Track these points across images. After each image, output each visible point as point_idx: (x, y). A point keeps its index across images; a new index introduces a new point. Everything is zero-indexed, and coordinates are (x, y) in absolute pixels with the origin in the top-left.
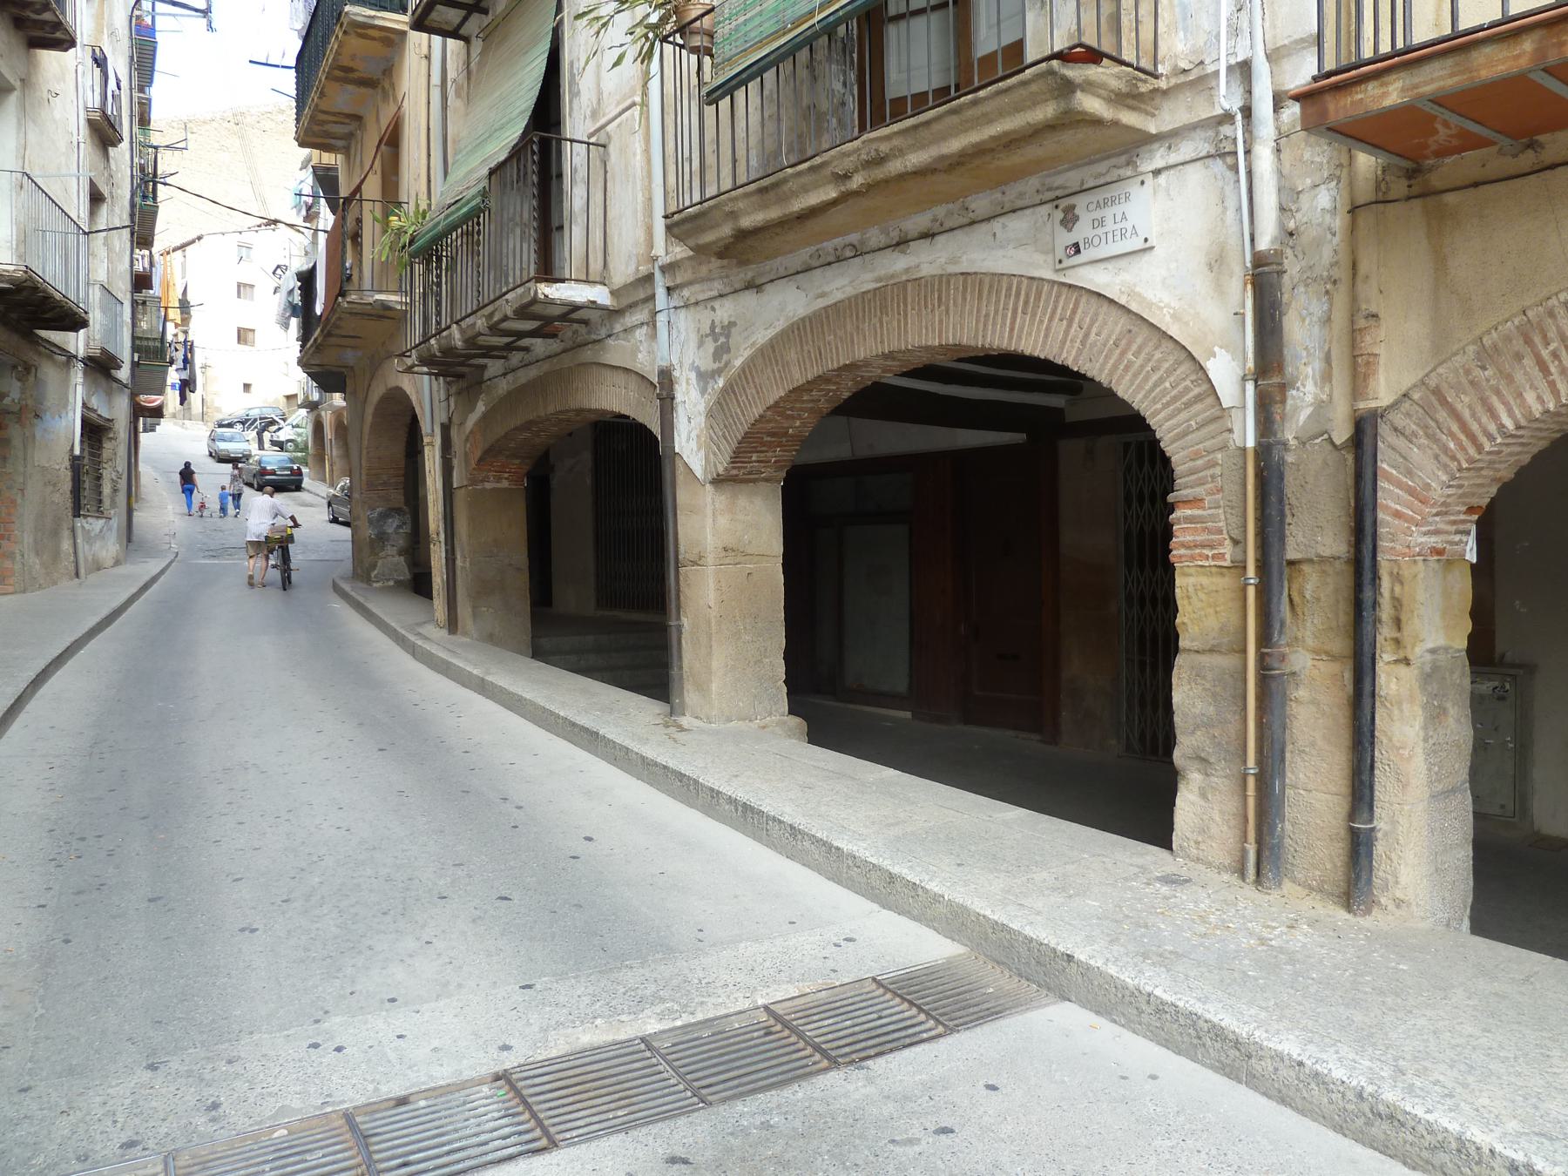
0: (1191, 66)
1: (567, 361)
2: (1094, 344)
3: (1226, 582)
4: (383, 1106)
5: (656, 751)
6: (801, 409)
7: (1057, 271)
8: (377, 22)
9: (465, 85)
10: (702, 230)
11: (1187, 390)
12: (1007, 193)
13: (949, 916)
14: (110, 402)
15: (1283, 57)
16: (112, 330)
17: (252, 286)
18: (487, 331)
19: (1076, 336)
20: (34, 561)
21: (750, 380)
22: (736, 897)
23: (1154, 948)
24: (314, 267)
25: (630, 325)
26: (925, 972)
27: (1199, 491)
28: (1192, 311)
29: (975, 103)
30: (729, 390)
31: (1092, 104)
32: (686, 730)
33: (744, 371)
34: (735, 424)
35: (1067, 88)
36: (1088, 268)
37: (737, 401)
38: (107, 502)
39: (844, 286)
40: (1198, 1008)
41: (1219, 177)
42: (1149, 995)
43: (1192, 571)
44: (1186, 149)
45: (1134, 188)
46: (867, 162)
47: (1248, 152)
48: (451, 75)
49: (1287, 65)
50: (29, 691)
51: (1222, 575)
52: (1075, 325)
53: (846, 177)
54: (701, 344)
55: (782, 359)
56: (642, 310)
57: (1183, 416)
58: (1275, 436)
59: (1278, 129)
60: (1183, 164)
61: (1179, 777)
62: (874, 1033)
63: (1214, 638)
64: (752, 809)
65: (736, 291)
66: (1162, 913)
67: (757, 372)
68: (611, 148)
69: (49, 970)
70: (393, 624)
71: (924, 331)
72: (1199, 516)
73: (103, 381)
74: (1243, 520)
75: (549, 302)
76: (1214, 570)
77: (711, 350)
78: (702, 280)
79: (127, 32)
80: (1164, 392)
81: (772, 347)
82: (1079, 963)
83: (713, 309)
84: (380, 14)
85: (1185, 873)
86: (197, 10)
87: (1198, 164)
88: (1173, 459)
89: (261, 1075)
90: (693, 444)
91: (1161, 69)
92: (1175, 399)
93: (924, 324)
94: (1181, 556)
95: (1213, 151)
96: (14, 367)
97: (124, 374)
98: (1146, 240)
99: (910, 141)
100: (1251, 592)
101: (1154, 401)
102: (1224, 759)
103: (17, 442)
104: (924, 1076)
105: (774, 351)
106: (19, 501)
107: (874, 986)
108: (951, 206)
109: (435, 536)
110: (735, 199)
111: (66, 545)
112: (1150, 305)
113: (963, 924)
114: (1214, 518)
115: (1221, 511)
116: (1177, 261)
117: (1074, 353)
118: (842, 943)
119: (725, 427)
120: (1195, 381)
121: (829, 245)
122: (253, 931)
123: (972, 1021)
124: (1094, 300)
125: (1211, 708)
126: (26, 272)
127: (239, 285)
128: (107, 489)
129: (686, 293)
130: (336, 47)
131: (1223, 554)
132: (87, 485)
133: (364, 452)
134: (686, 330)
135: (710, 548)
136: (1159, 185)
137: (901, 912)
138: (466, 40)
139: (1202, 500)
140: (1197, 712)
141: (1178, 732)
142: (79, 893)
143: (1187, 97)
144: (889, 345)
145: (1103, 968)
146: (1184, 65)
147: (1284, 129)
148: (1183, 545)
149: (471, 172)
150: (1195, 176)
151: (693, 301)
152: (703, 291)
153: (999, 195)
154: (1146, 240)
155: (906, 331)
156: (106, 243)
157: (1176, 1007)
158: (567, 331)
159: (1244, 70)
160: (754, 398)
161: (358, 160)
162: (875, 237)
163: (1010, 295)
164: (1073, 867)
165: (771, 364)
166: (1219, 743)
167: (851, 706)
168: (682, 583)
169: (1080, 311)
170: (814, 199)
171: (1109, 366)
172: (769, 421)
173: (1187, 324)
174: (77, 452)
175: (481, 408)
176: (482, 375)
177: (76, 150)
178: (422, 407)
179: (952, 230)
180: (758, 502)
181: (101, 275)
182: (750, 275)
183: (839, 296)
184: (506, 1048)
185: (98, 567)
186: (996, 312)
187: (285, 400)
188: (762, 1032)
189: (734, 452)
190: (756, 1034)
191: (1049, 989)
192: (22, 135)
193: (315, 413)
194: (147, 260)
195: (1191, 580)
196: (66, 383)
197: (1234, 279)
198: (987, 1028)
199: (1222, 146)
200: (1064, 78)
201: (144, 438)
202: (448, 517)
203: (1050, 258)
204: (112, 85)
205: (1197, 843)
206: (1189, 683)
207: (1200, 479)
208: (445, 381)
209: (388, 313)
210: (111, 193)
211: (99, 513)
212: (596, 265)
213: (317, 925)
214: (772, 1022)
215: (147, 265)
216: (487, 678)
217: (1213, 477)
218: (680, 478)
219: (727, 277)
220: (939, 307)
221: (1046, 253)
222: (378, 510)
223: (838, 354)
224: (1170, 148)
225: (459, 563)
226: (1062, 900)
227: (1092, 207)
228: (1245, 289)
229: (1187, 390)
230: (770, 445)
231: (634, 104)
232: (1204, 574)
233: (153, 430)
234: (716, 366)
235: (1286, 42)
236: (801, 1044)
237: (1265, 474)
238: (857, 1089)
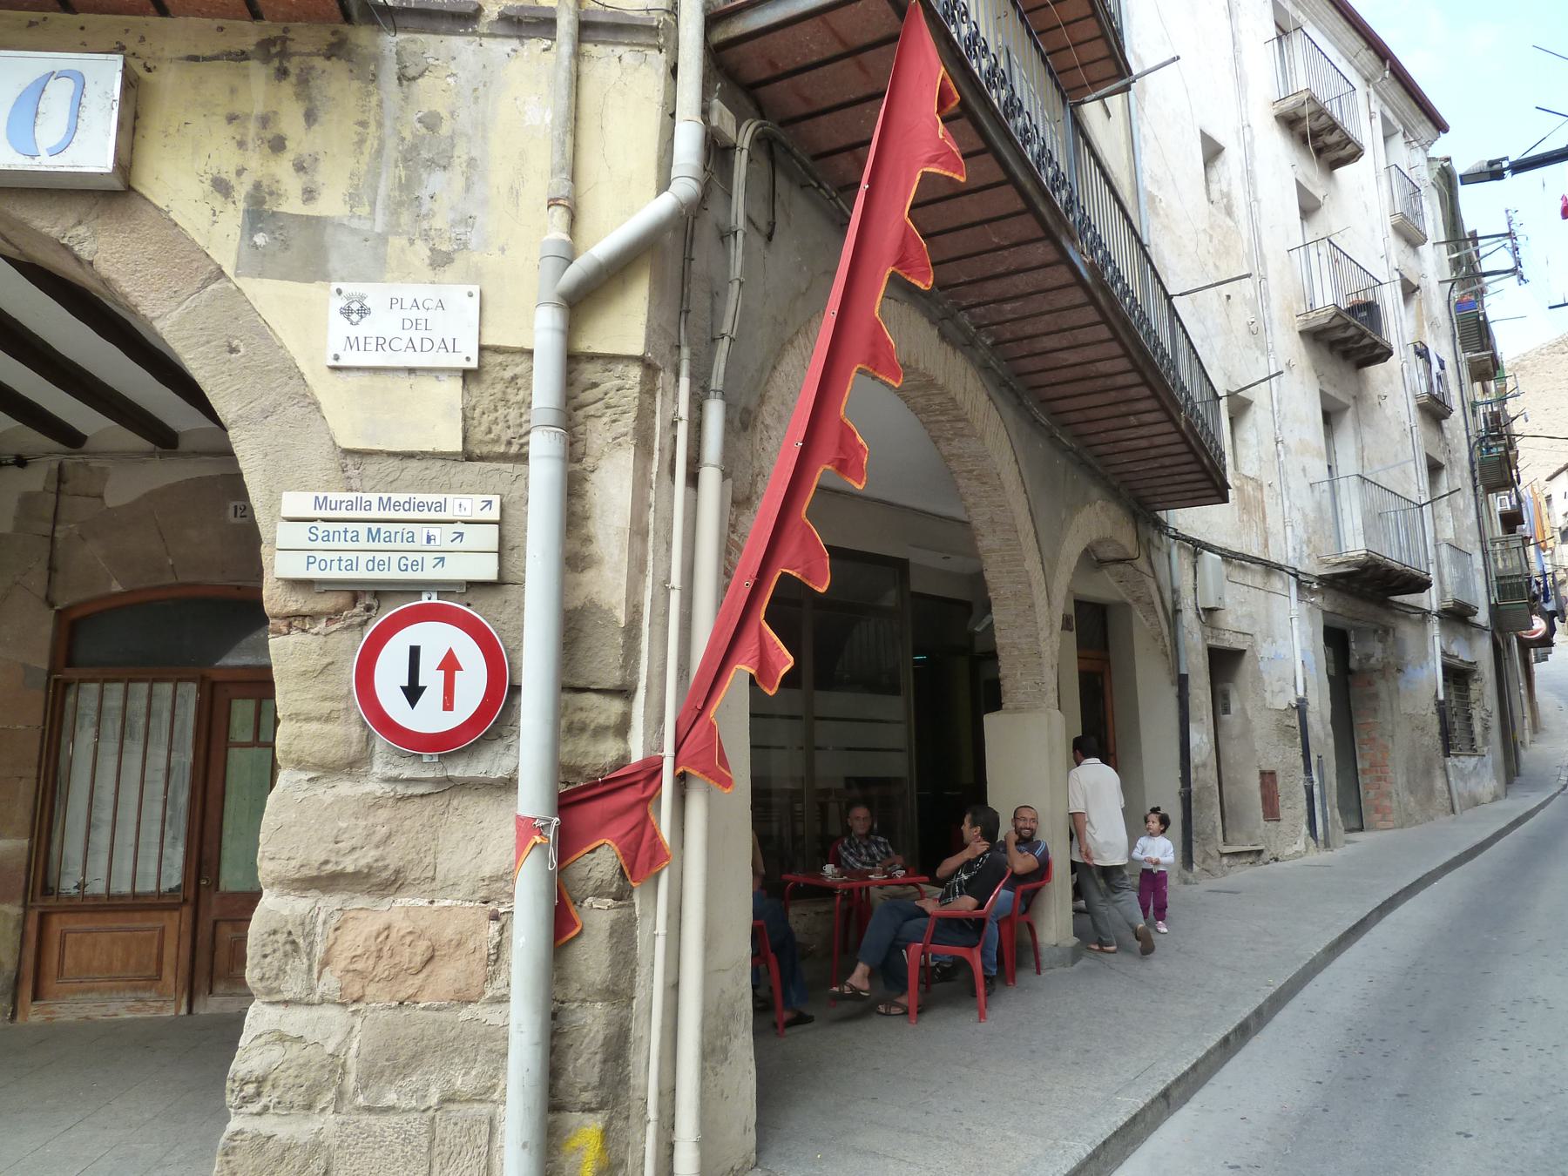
14: (1471, 647)
16: (1464, 582)
38: (1479, 740)
50: (1374, 915)
69: (1305, 1127)
73: (1462, 629)
96: (1376, 631)
97: (1482, 617)
103: (1384, 695)
106: (1390, 746)
111: (1439, 783)
128: (1478, 728)
132: (1457, 726)
142: (1350, 1079)
156: (1450, 504)
174: (1441, 697)
177: (1410, 435)
181: (1448, 533)
185: (1475, 802)
194: (1514, 499)
196: (1424, 637)
201: (1538, 668)
204: (1436, 367)
210: (1449, 459)
211: (1473, 750)
215: (1514, 502)
233: (1546, 660)
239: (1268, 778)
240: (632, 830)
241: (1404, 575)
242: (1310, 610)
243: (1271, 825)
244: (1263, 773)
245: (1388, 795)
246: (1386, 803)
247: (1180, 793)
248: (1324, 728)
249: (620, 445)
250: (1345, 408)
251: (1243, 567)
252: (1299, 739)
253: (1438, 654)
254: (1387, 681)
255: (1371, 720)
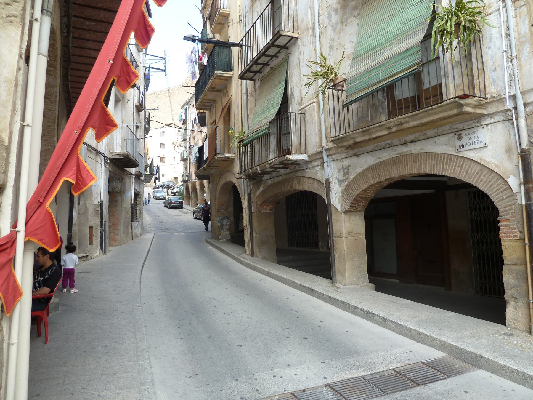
0: (497, 96)
1: (292, 175)
2: (469, 174)
3: (518, 244)
4: (300, 392)
5: (332, 294)
6: (372, 190)
7: (457, 152)
8: (224, 75)
9: (254, 94)
10: (343, 142)
11: (501, 187)
12: (439, 130)
13: (440, 344)
15: (526, 93)
17: (164, 144)
18: (269, 168)
19: (464, 171)
20: (123, 236)
21: (356, 182)
22: (372, 338)
23: (507, 354)
24: (203, 145)
25: (314, 166)
26: (436, 361)
27: (508, 217)
28: (501, 164)
29: (432, 109)
30: (349, 185)
31: (468, 109)
32: (339, 288)
33: (354, 180)
34: (351, 195)
35: (461, 105)
36: (467, 151)
37: (352, 189)
39: (386, 156)
40: (525, 371)
41: (508, 126)
42: (509, 367)
43: (507, 240)
44: (496, 118)
45: (480, 129)
46: (397, 124)
47: (517, 119)
48: (249, 90)
49: (527, 96)
51: (517, 242)
52: (463, 168)
53: (391, 128)
54: (339, 172)
55: (366, 176)
56: (318, 161)
57: (501, 195)
58: (532, 201)
59: (526, 113)
60: (496, 122)
61: (507, 303)
62: (426, 377)
63: (516, 261)
64: (370, 313)
65: (350, 157)
66: (507, 344)
67: (358, 180)
68: (307, 114)
70: (232, 254)
71: (413, 169)
72: (508, 224)
74: (522, 226)
75: (290, 160)
76: (514, 240)
77: (343, 174)
78: (339, 153)
79: (143, 78)
80: (494, 188)
81: (363, 173)
82: (485, 358)
83: (343, 162)
84: (225, 73)
85: (511, 332)
86: (162, 70)
87: (501, 122)
88: (498, 207)
89: (265, 383)
90: (337, 201)
91: (487, 96)
92: (498, 190)
93: (413, 167)
94: (503, 236)
95: (505, 119)
98: (485, 144)
99: (411, 119)
100: (527, 247)
101: (491, 190)
102: (522, 297)
103: (119, 201)
104: (445, 388)
105: (363, 174)
106: (120, 218)
107: (422, 364)
108: (421, 133)
109: (246, 227)
110: (355, 134)
111: (130, 231)
112: (488, 162)
113: (445, 347)
114: (513, 225)
115: (515, 223)
116: (496, 150)
117: (464, 176)
118: (409, 352)
119: (348, 196)
120: (504, 185)
121: (381, 144)
122: (241, 346)
123: (455, 374)
124: (469, 161)
125: (516, 282)
126: (127, 153)
127: (161, 144)
129: (333, 157)
130: (211, 82)
131: (517, 236)
133: (217, 200)
134: (334, 168)
135: (344, 232)
136: (489, 128)
137: (423, 343)
138: (254, 80)
139: (509, 220)
140: (512, 283)
141: (505, 289)
143: (496, 104)
144: (402, 173)
145: (493, 359)
146: (494, 95)
147: (527, 113)
148: (503, 233)
149: (260, 121)
150: (500, 126)
151: (336, 159)
152: (339, 156)
153: (437, 130)
154: (485, 144)
155: (407, 169)
157: (518, 370)
158: (292, 167)
159: (514, 97)
160: (357, 188)
161: (214, 112)
162: (396, 141)
163: (441, 159)
164: (475, 330)
165: (363, 178)
166: (519, 293)
167: (377, 278)
168: (334, 243)
169: (465, 164)
170: (380, 134)
171: (475, 180)
172: (362, 194)
173: (500, 168)
174: (133, 202)
175: (262, 188)
176: (262, 179)
178: (240, 188)
179: (421, 140)
180: (357, 218)
182: (355, 152)
183: (385, 158)
184: (325, 378)
186: (437, 164)
187: (174, 179)
188: (394, 376)
189: (351, 204)
190: (392, 377)
191: (475, 366)
192: (122, 113)
193: (186, 183)
195: (507, 243)
197: (515, 155)
198: (460, 376)
199: (508, 117)
200: (459, 103)
202: (251, 220)
203: (454, 148)
205: (514, 323)
206: (508, 274)
207: (508, 213)
208: (249, 181)
209: (229, 160)
212: (303, 148)
213: (258, 345)
214: (396, 373)
216: (270, 271)
217: (512, 213)
218: (333, 211)
219: (347, 152)
220: (418, 162)
221: (453, 147)
222: (221, 217)
223: (385, 176)
224: (491, 118)
225: (254, 235)
226: (475, 340)
227: (467, 134)
228: (518, 159)
229: (501, 187)
230: (361, 201)
231: (314, 102)
232: (511, 242)
234: (344, 178)
235: (527, 90)
236: (407, 379)
237: (529, 213)
238: (427, 391)
239: (91, 228)
240: (5, 281)
241: (134, 161)
242: (106, 170)
243: (91, 246)
244: (90, 227)
245: (117, 234)
246: (116, 237)
247: (68, 235)
248: (106, 211)
249: (11, 22)
250: (120, 100)
251: (90, 151)
252: (100, 215)
253: (133, 188)
254: (121, 196)
255: (114, 209)
